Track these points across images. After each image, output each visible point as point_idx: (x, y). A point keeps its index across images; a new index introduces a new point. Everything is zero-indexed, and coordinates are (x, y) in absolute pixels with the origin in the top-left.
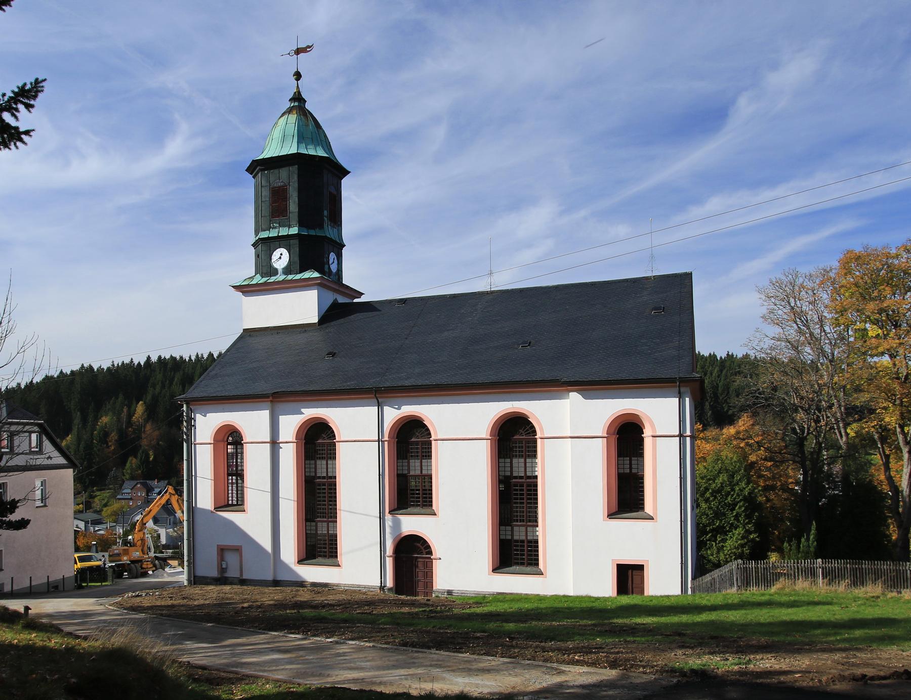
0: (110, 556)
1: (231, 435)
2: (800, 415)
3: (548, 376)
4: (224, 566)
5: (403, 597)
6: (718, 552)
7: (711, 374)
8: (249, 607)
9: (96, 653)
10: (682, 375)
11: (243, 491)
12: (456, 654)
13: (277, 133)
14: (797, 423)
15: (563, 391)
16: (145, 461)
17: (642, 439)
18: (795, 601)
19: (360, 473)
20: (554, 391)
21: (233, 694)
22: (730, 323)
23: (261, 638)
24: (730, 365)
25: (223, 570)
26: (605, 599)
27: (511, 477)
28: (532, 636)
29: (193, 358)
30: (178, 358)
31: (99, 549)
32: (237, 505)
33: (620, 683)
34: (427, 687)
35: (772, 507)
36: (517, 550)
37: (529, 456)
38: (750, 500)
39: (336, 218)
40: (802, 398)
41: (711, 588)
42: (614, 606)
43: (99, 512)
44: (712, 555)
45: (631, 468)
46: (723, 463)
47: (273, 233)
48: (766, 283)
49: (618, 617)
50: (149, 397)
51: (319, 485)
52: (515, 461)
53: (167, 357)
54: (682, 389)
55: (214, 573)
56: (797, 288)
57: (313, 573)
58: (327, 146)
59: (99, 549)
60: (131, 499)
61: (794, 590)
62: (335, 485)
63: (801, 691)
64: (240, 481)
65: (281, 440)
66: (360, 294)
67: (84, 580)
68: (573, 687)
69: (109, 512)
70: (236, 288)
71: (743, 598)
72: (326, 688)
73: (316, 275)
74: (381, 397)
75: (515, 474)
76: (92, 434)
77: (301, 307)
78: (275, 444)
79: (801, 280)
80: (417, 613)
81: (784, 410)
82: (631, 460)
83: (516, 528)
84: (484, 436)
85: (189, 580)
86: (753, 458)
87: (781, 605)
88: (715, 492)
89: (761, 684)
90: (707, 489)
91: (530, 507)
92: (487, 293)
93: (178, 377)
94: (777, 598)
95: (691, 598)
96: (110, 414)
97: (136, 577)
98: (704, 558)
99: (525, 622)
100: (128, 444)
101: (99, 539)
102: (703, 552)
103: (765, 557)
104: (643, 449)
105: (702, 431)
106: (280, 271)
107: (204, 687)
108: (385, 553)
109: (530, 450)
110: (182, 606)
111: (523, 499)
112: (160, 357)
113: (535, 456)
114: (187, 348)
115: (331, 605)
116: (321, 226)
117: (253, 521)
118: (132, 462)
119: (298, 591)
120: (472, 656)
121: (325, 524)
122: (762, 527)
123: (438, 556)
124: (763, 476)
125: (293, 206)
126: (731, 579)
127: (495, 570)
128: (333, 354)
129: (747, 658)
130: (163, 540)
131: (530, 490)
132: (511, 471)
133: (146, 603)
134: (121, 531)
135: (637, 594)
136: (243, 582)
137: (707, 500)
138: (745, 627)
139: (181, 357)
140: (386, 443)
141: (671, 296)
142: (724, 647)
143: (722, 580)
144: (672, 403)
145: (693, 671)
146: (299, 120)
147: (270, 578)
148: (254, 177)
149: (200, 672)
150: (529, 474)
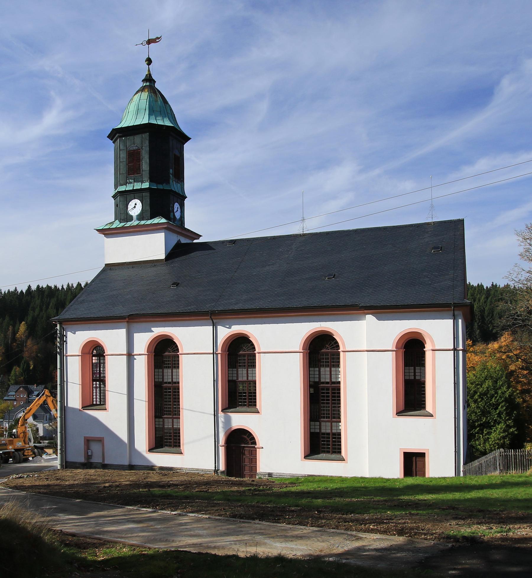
1: (95, 348)
3: (349, 302)
4: (90, 454)
6: (484, 443)
7: (479, 300)
8: (110, 486)
10: (456, 301)
11: (104, 393)
12: (275, 524)
13: (132, 107)
16: (27, 370)
17: (423, 354)
21: (96, 556)
24: (494, 293)
25: (88, 457)
26: (395, 480)
27: (319, 382)
28: (336, 509)
29: (65, 287)
30: (53, 287)
32: (100, 405)
34: (252, 550)
35: (527, 407)
39: (180, 176)
41: (479, 471)
42: (401, 486)
44: (480, 445)
45: (415, 376)
46: (488, 371)
47: (129, 187)
49: (404, 495)
50: (30, 318)
51: (166, 389)
52: (322, 369)
54: (456, 313)
55: (82, 459)
57: (161, 460)
60: (15, 400)
64: (102, 386)
65: (135, 353)
66: (198, 236)
71: (505, 479)
72: (171, 551)
73: (164, 220)
75: (322, 380)
77: (151, 246)
78: (130, 356)
80: (244, 492)
82: (415, 370)
83: (323, 424)
85: (62, 465)
86: (512, 367)
88: (482, 395)
89: (519, 547)
90: (475, 392)
92: (300, 235)
93: (53, 301)
95: (462, 479)
98: (474, 447)
99: (330, 498)
102: (473, 443)
103: (522, 446)
104: (424, 360)
105: (472, 346)
106: (135, 218)
110: (56, 485)
112: (38, 286)
113: (338, 366)
114: (60, 279)
116: (168, 182)
117: (112, 418)
118: (16, 370)
119: (148, 473)
120: (288, 526)
121: (170, 420)
122: (519, 423)
123: (261, 446)
124: (521, 382)
125: (145, 166)
126: (495, 464)
128: (177, 284)
130: (41, 433)
131: (335, 393)
132: (320, 378)
134: (7, 425)
135: (420, 476)
136: (105, 466)
137: (476, 401)
138: (505, 502)
139: (56, 287)
140: (219, 355)
141: (448, 238)
142: (489, 518)
145: (464, 537)
146: (150, 97)
147: (126, 463)
148: (114, 142)
150: (333, 380)
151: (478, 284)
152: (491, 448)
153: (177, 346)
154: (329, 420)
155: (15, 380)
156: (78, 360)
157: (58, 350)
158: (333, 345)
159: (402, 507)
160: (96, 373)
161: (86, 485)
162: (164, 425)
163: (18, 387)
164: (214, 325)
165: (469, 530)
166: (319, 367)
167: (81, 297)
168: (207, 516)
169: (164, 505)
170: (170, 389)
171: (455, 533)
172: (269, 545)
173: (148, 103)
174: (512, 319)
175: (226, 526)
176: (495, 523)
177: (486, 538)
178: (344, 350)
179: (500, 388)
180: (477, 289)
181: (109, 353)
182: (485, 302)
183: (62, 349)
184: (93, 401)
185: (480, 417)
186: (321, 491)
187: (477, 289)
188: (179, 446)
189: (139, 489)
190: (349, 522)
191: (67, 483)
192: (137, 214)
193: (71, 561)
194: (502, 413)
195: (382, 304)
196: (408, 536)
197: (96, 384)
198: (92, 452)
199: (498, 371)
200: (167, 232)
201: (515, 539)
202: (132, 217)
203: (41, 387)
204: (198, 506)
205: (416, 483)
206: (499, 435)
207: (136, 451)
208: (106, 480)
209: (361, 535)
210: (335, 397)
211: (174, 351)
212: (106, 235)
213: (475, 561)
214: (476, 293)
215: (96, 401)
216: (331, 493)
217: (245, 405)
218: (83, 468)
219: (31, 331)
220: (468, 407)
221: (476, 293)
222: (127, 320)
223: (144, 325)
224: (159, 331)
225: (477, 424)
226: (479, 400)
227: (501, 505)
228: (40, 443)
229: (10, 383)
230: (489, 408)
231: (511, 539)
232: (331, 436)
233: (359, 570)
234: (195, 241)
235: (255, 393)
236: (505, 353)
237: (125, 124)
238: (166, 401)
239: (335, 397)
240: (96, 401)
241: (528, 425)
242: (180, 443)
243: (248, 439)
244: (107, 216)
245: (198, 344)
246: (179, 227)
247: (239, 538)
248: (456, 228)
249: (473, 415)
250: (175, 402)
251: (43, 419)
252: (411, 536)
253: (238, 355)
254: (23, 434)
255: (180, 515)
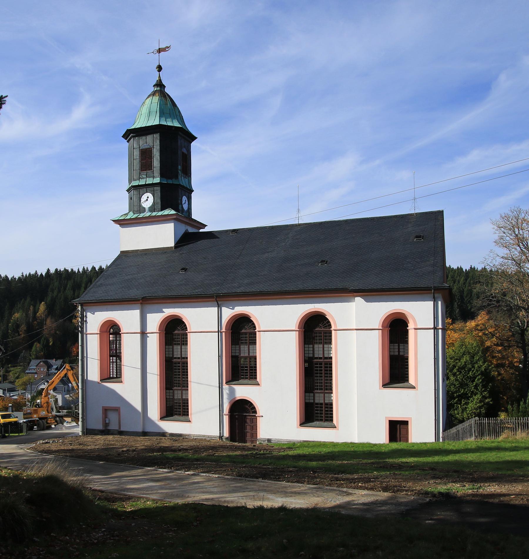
0: (24, 414)
1: (112, 327)
2: (522, 313)
3: (340, 286)
4: (107, 422)
5: (236, 444)
6: (462, 412)
7: (459, 282)
8: (128, 450)
9: (36, 479)
10: (435, 285)
11: (120, 367)
12: (276, 482)
13: (145, 110)
14: (519, 319)
15: (350, 296)
16: (46, 346)
17: (407, 332)
18: (515, 447)
19: (205, 355)
20: (343, 296)
21: (125, 508)
22: (471, 245)
23: (139, 472)
24: (472, 276)
25: (106, 425)
26: (381, 445)
27: (313, 358)
28: (329, 470)
29: (81, 270)
30: (70, 270)
31: (14, 409)
32: (117, 377)
33: (389, 502)
34: (258, 503)
35: (502, 379)
36: (317, 410)
37: (326, 343)
38: (486, 375)
39: (187, 171)
40: (524, 301)
41: (457, 437)
42: (387, 450)
43: (12, 383)
44: (458, 414)
45: (399, 352)
46: (466, 347)
47: (142, 182)
48: (498, 217)
49: (389, 458)
50: (49, 299)
51: (176, 363)
52: (316, 346)
53: (62, 270)
54: (436, 295)
55: (100, 427)
56: (520, 221)
57: (171, 427)
58: (181, 119)
59: (14, 409)
60: (36, 373)
61: (516, 439)
62: (187, 364)
63: (515, 506)
64: (118, 361)
65: (148, 331)
66: (204, 226)
67: (7, 432)
68: (357, 504)
69: (20, 383)
70: (115, 221)
71: (479, 444)
72: (188, 504)
73: (173, 212)
74: (220, 301)
75: (316, 356)
76: (8, 326)
77: (162, 236)
78: (144, 334)
79: (523, 215)
80: (246, 455)
81: (511, 309)
82: (399, 346)
83: (317, 395)
84: (294, 329)
85: (83, 432)
86: (488, 344)
87: (505, 449)
88: (460, 369)
89: (487, 502)
90: (454, 366)
91: (327, 380)
92: (296, 225)
93: (70, 284)
94: (503, 445)
95: (442, 444)
96: (21, 311)
97: (43, 430)
98: (453, 416)
99: (324, 461)
100: (34, 332)
101: (14, 402)
102: (452, 412)
103: (496, 415)
104: (408, 338)
105: (452, 324)
106: (147, 209)
107: (106, 503)
108: (223, 412)
109: (327, 339)
110: (79, 450)
111: (322, 373)
112: (56, 270)
113: (330, 343)
114: (76, 263)
115: (186, 450)
116: (176, 177)
117: (128, 389)
118: (37, 346)
119: (161, 439)
120: (287, 484)
121: (180, 392)
122: (494, 394)
123: (261, 415)
124: (496, 357)
125: (156, 163)
126: (470, 431)
127: (302, 424)
128: (184, 269)
129: (479, 485)
130: (60, 403)
131: (327, 367)
132: (313, 354)
133: (54, 447)
134: (29, 396)
135: (404, 441)
136: (121, 433)
137: (454, 375)
138: (477, 464)
139: (72, 270)
140: (224, 334)
141: (428, 228)
142: (463, 478)
143: (464, 431)
144: (429, 305)
145: (440, 493)
146: (160, 100)
147: (140, 430)
148: (128, 142)
149: (100, 494)
150: (326, 356)
151: (458, 267)
152: (469, 417)
153: (185, 325)
154: (180, 388)
155: (36, 355)
156: (97, 337)
157: (80, 329)
158: (325, 324)
159: (387, 468)
160: (112, 349)
161: (106, 449)
162: (173, 396)
163: (39, 361)
164: (219, 306)
165: (445, 487)
166: (313, 344)
167: (100, 281)
168: (217, 476)
169: (177, 466)
170: (179, 363)
171: (432, 490)
172: (272, 499)
173: (158, 106)
174: (488, 300)
175: (233, 484)
176: (468, 482)
177: (459, 494)
178: (336, 329)
179: (477, 363)
180: (457, 272)
181: (124, 331)
182: (464, 283)
183: (82, 328)
184: (110, 375)
185: (459, 389)
186: (315, 454)
187: (457, 272)
188: (188, 415)
189: (153, 453)
190: (340, 481)
191: (89, 448)
192: (149, 206)
193: (105, 511)
194: (479, 385)
195: (370, 288)
196: (392, 492)
197: (113, 359)
198: (109, 420)
199: (475, 347)
200: (176, 222)
201: (484, 495)
202: (144, 208)
203: (59, 362)
204: (208, 467)
205: (400, 448)
206: (476, 405)
207: (149, 419)
208: (124, 445)
209: (350, 491)
210: (327, 370)
211: (182, 330)
212: (121, 225)
213: (448, 513)
214: (456, 275)
215: (113, 375)
216: (324, 456)
217: (247, 378)
218: (102, 435)
219: (50, 310)
220: (447, 380)
221: (456, 275)
222: (141, 301)
223: (156, 306)
224: (169, 311)
225: (455, 395)
226: (458, 373)
227: (474, 467)
228: (60, 412)
229: (31, 358)
230: (467, 381)
231: (482, 495)
232: (323, 406)
233: (350, 518)
234: (201, 230)
235: (256, 367)
236: (481, 330)
237: (137, 125)
238: (176, 375)
239: (327, 370)
240: (113, 375)
241: (503, 396)
242: (188, 412)
243: (250, 409)
244: (122, 207)
245: (204, 323)
246: (187, 218)
247: (245, 494)
248: (437, 218)
249: (452, 387)
250: (184, 375)
251: (62, 391)
252: (394, 492)
253: (241, 332)
254: (46, 404)
255: (193, 475)
